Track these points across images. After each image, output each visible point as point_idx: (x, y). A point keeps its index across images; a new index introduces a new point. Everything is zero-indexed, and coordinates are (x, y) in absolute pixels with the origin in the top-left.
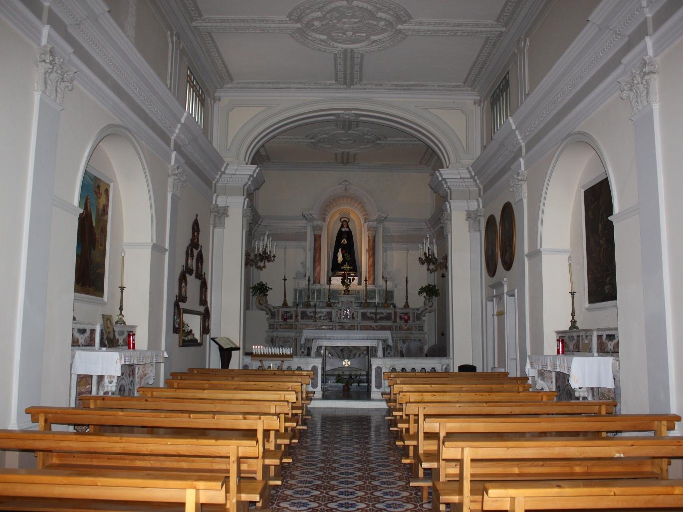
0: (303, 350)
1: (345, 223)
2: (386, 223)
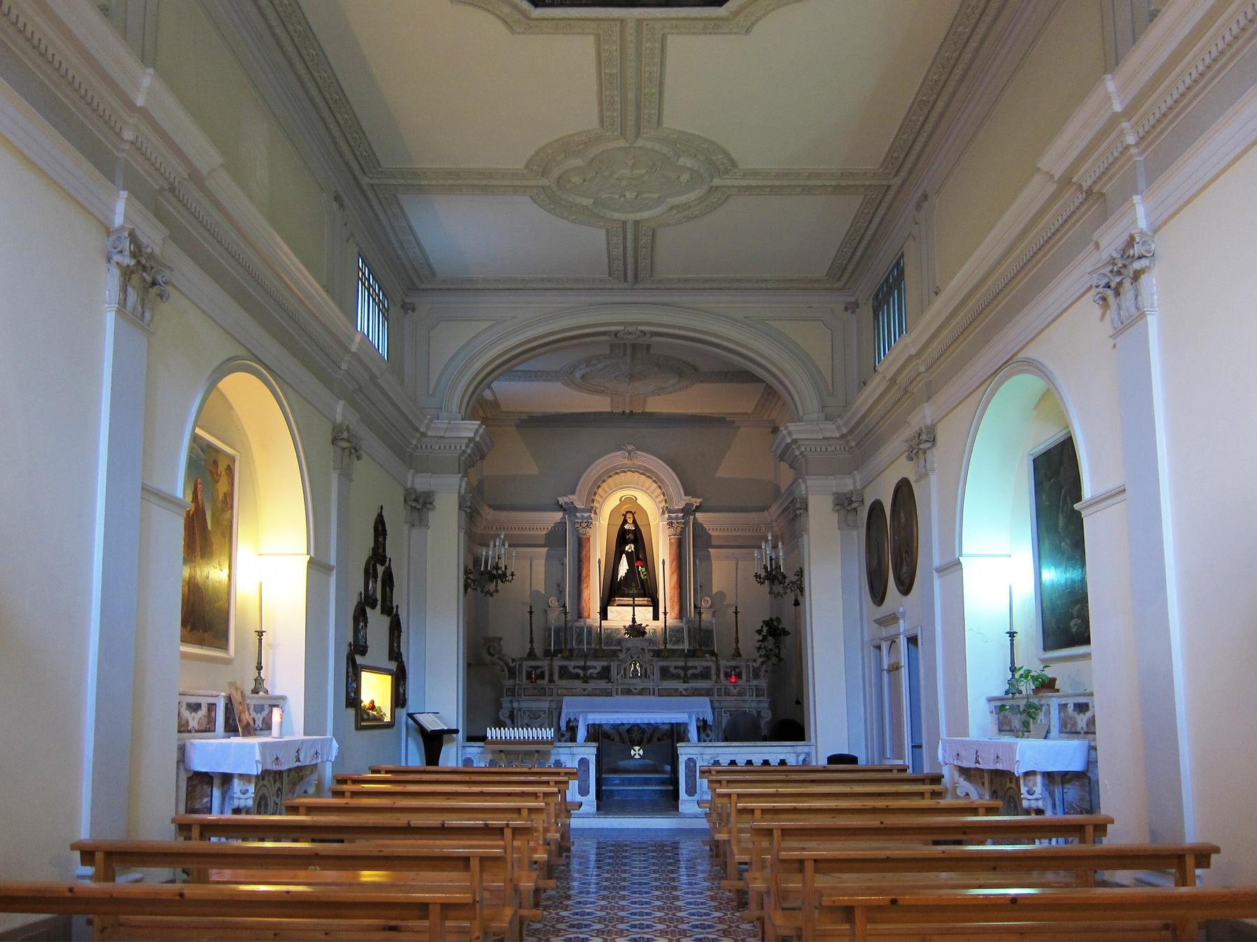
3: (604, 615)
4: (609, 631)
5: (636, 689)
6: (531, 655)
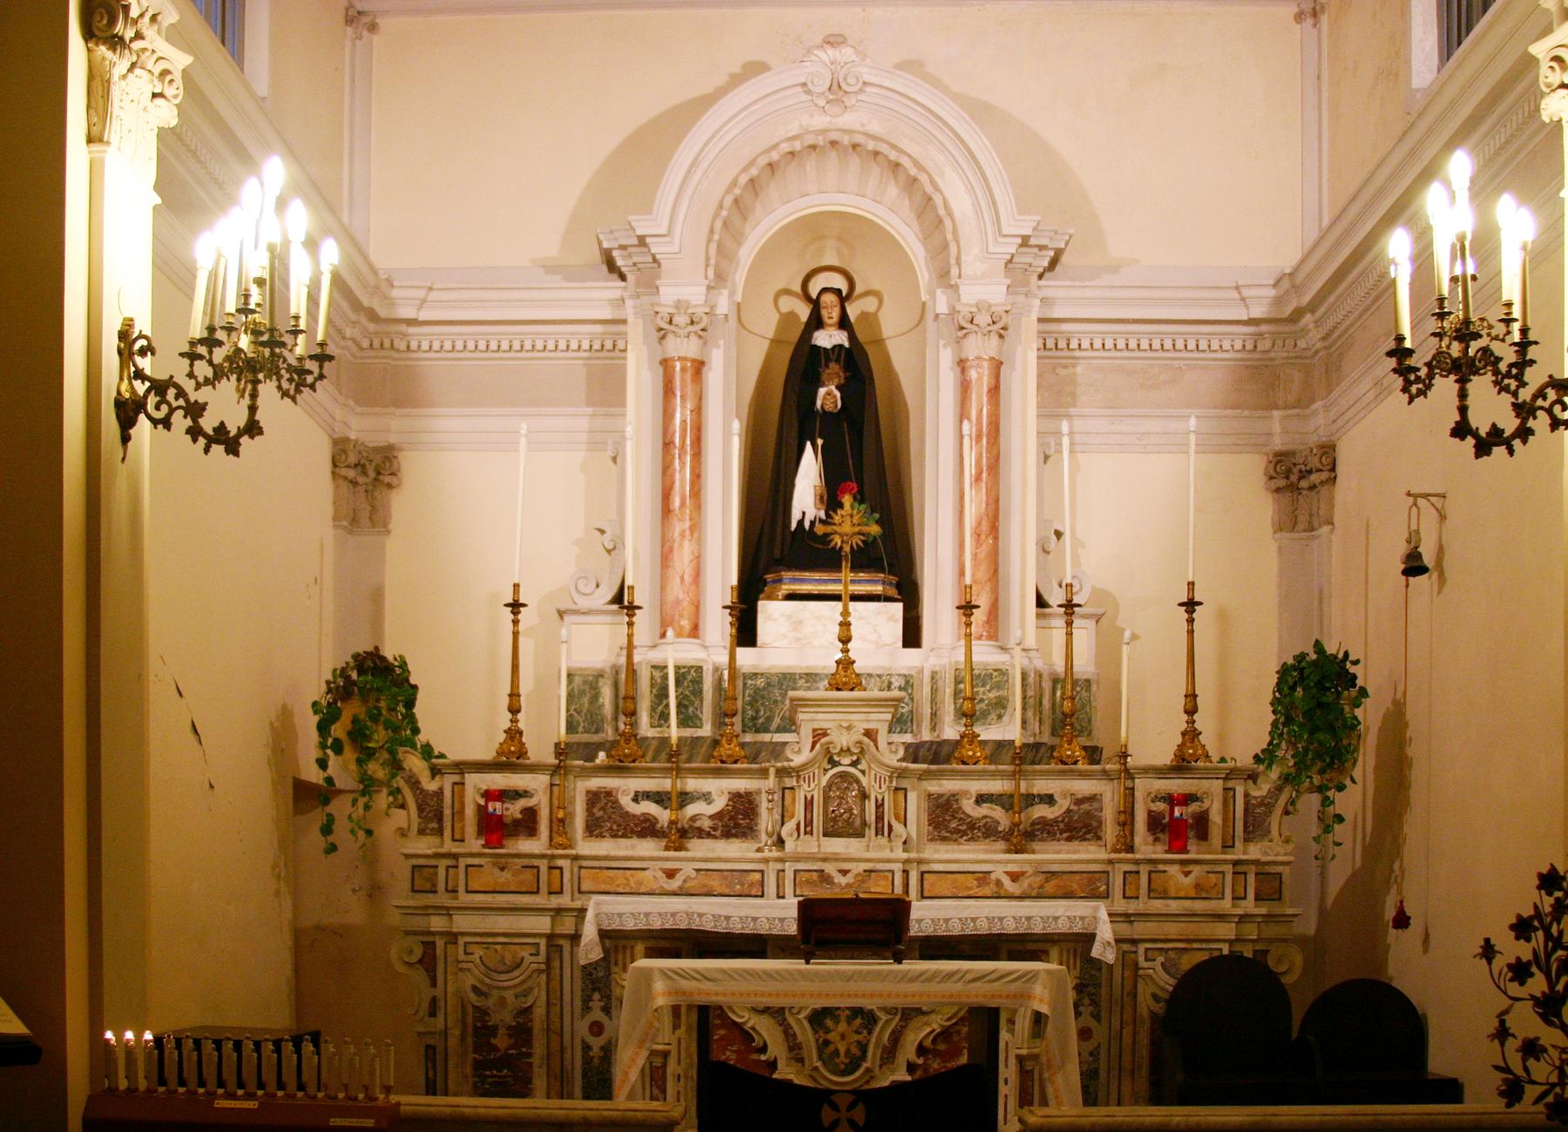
1: (829, 299)
3: (746, 633)
4: (760, 682)
5: (844, 872)
6: (512, 757)
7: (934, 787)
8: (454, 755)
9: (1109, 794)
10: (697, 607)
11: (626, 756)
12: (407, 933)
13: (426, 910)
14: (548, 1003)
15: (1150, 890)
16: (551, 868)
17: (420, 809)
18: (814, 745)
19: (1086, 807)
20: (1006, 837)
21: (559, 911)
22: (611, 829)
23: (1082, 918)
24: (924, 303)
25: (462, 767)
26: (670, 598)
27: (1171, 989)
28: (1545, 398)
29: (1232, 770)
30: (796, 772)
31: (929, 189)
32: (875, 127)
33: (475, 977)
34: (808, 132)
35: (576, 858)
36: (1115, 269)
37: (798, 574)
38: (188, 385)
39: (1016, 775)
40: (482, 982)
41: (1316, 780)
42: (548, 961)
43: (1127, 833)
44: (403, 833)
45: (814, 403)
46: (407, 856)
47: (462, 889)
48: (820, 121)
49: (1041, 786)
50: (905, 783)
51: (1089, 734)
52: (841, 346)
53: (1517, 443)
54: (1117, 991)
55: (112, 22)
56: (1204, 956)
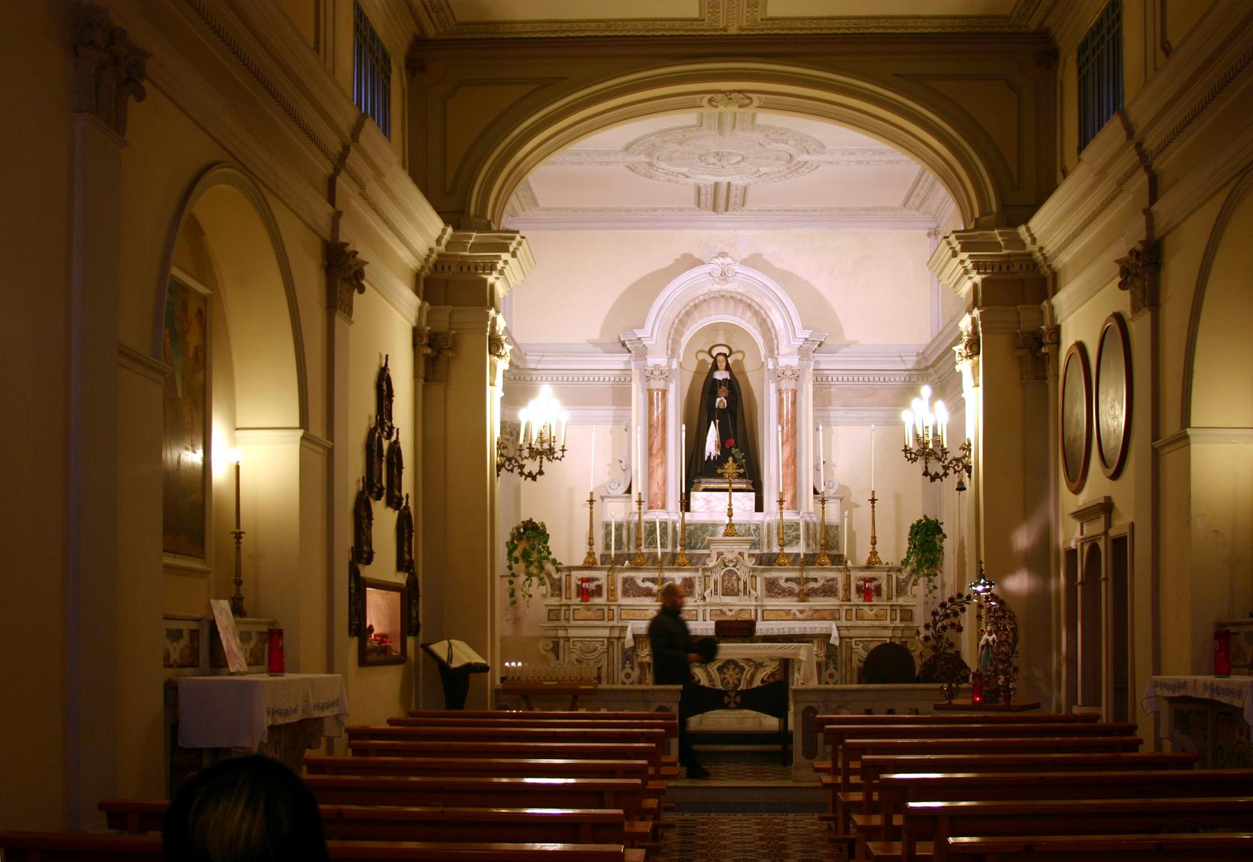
0: (628, 670)
1: (721, 358)
2: (819, 357)
3: (686, 506)
4: (692, 528)
5: (731, 610)
6: (590, 565)
7: (768, 575)
8: (565, 564)
9: (840, 577)
10: (664, 496)
11: (639, 563)
12: (546, 637)
13: (556, 628)
14: (608, 666)
15: (856, 617)
16: (609, 610)
17: (552, 586)
18: (717, 559)
19: (831, 583)
20: (798, 595)
21: (612, 628)
22: (633, 594)
23: (826, 628)
24: (763, 363)
25: (570, 569)
26: (653, 492)
27: (865, 657)
28: (952, 463)
29: (890, 568)
30: (711, 569)
31: (765, 316)
32: (740, 290)
33: (577, 655)
34: (711, 291)
35: (619, 605)
36: (848, 345)
37: (708, 480)
38: (519, 459)
39: (801, 570)
40: (581, 657)
41: (926, 571)
42: (608, 648)
43: (848, 593)
44: (544, 596)
45: (715, 404)
46: (546, 605)
47: (571, 618)
48: (716, 287)
49: (812, 574)
50: (755, 574)
51: (838, 549)
52: (726, 379)
53: (943, 478)
54: (844, 659)
55: (498, 349)
56: (879, 644)
